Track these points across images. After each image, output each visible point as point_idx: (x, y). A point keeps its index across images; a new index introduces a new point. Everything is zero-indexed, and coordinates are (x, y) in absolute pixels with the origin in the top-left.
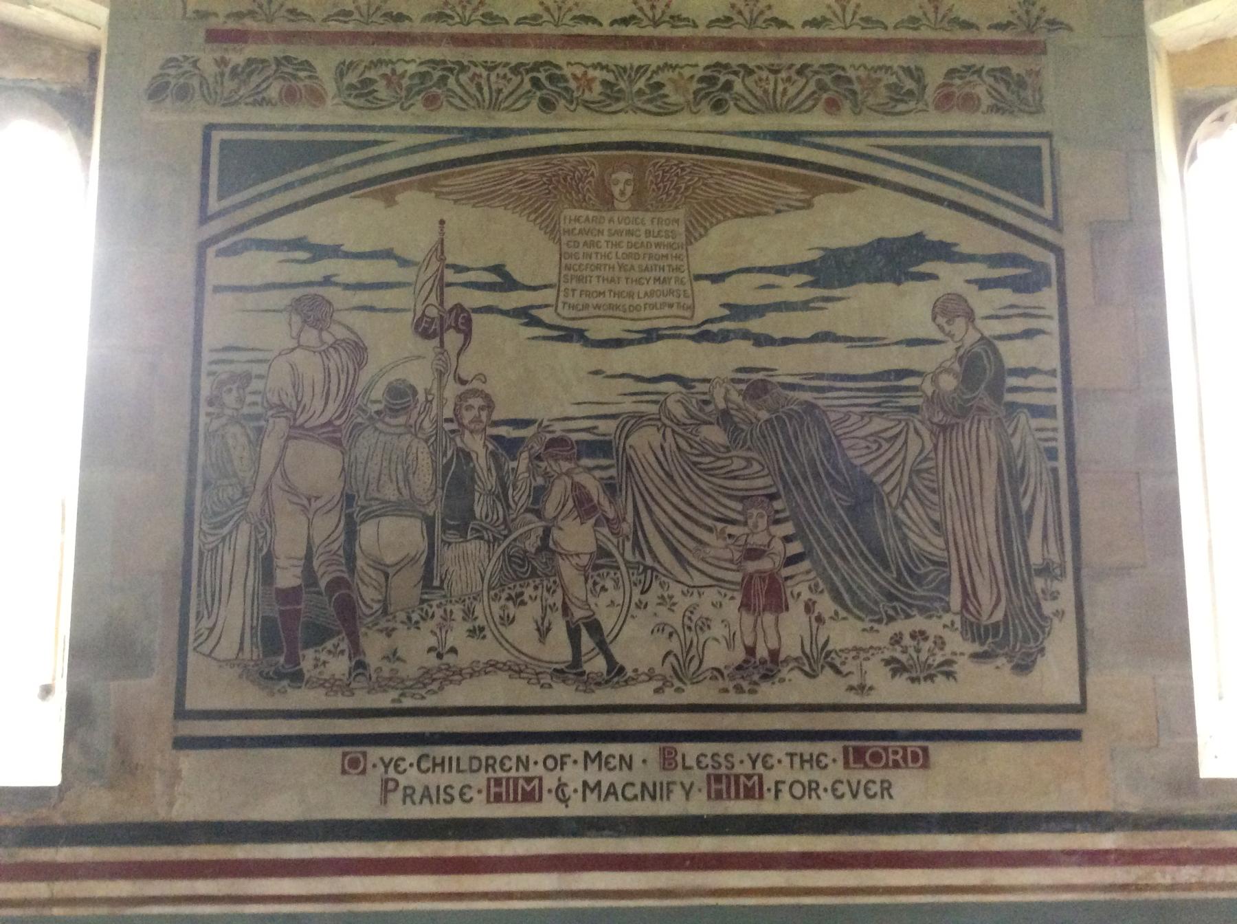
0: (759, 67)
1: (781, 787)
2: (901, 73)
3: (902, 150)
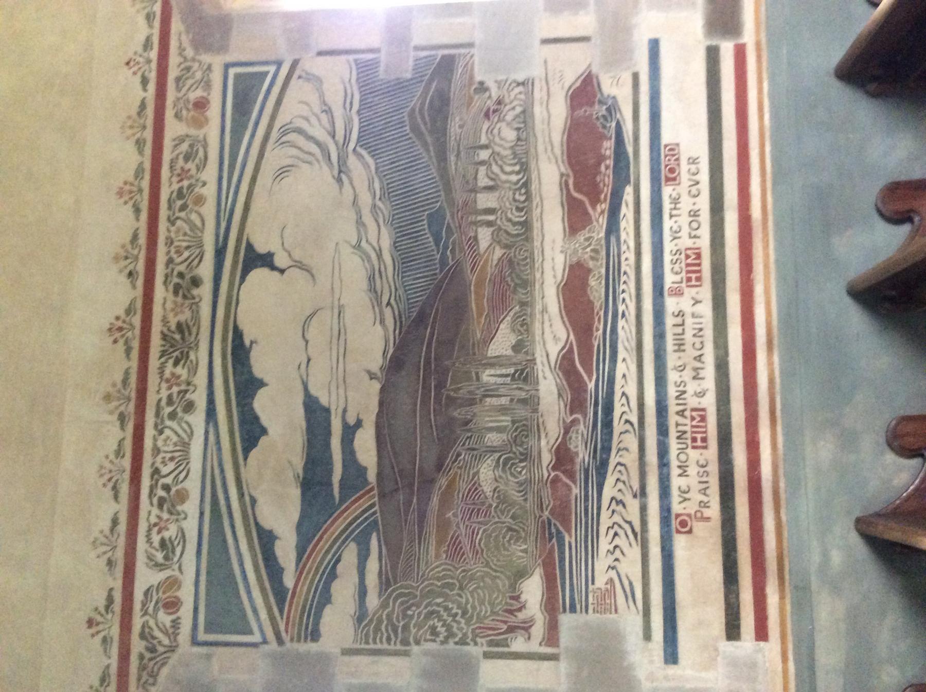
0: (169, 252)
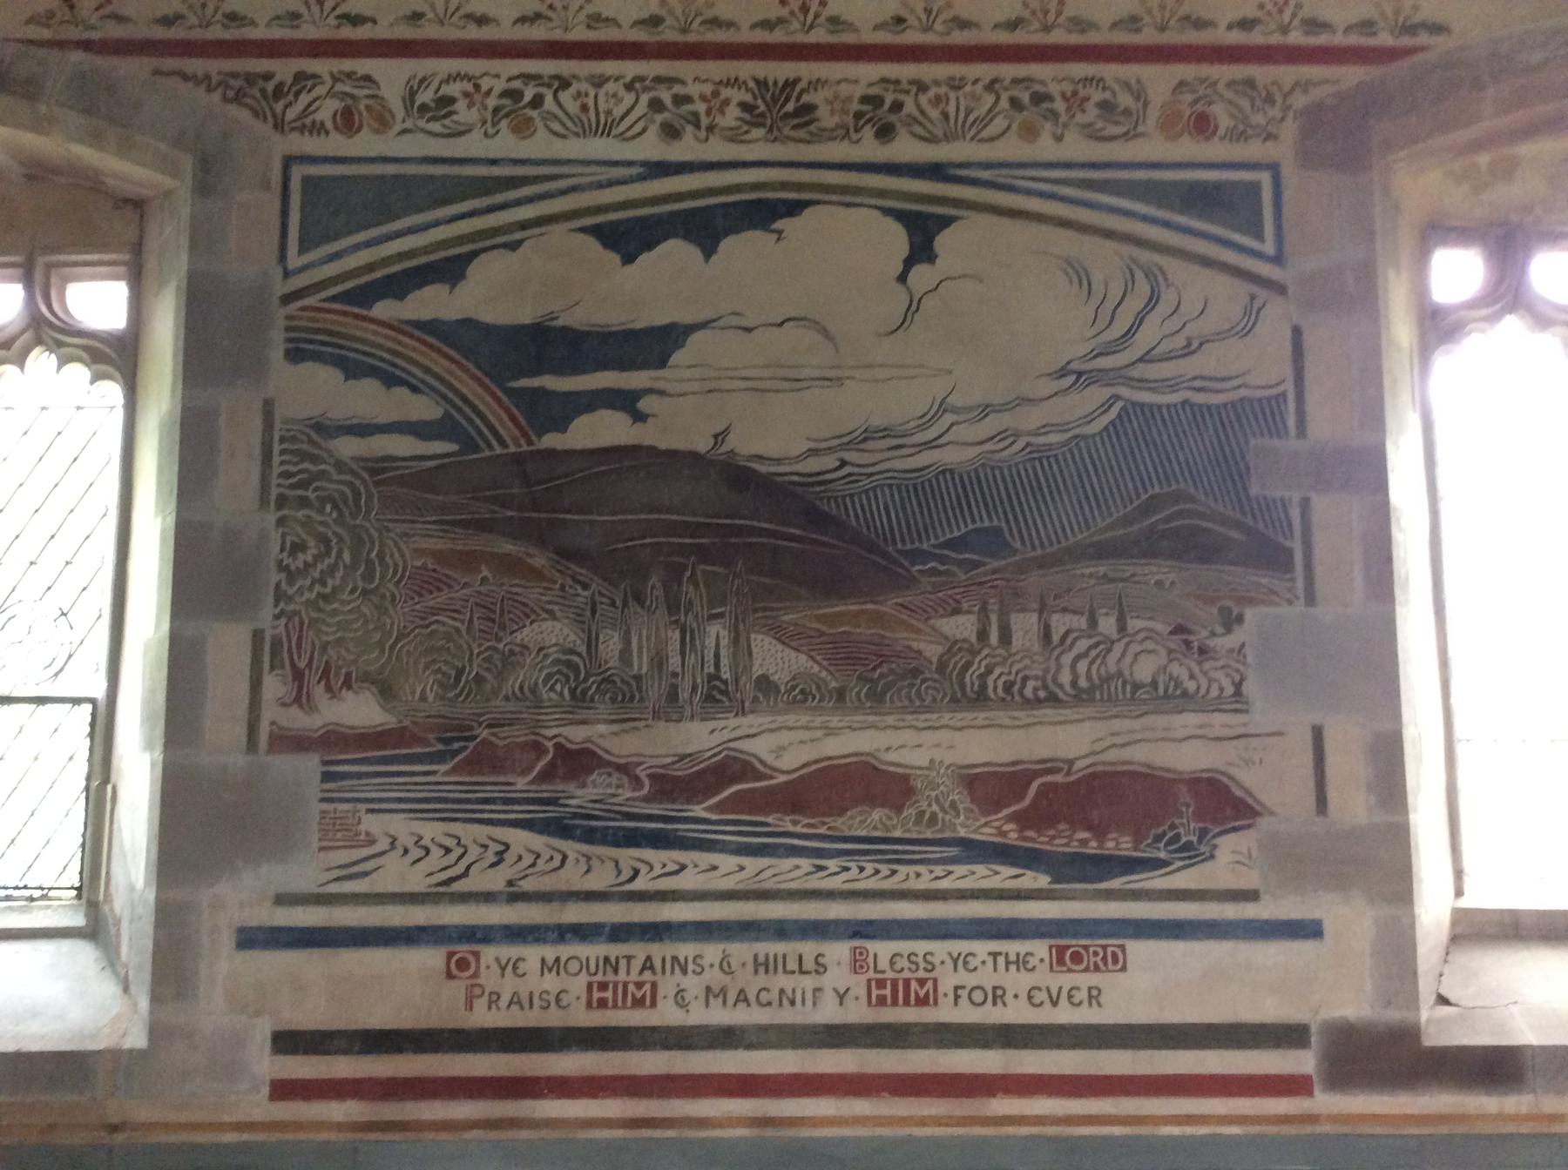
0: (937, 83)
1: (960, 992)
2: (1116, 88)
3: (537, 179)
